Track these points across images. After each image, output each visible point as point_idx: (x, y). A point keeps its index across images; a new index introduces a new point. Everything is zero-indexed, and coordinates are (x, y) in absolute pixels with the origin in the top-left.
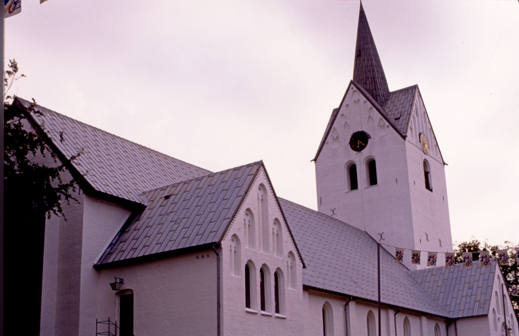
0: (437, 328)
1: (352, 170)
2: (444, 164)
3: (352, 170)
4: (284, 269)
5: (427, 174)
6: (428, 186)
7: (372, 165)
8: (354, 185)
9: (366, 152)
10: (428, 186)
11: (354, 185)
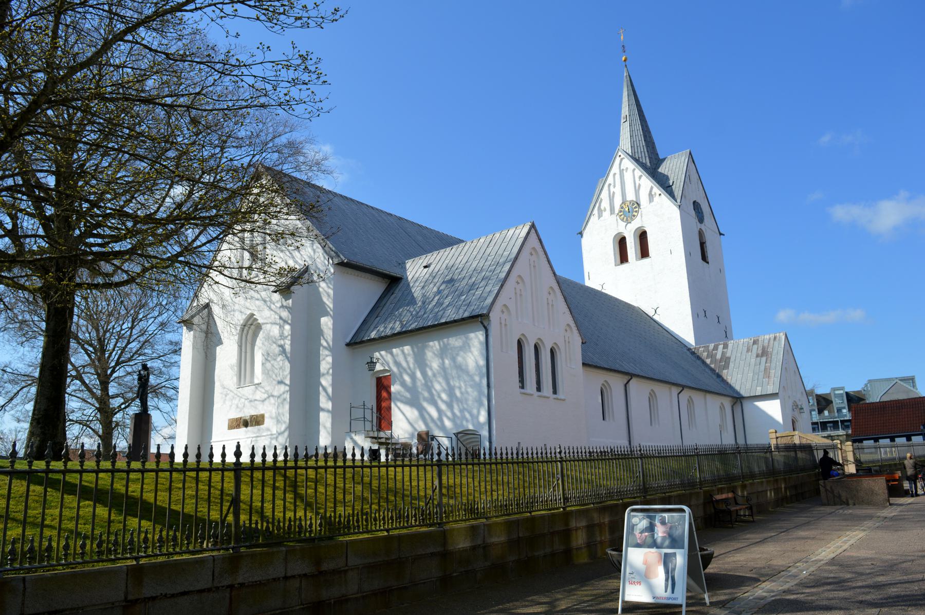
0: (722, 408)
1: (622, 243)
2: (721, 234)
3: (622, 243)
4: (561, 345)
5: (702, 245)
6: (704, 258)
7: (643, 237)
8: (623, 258)
9: (635, 224)
10: (704, 258)
11: (623, 258)
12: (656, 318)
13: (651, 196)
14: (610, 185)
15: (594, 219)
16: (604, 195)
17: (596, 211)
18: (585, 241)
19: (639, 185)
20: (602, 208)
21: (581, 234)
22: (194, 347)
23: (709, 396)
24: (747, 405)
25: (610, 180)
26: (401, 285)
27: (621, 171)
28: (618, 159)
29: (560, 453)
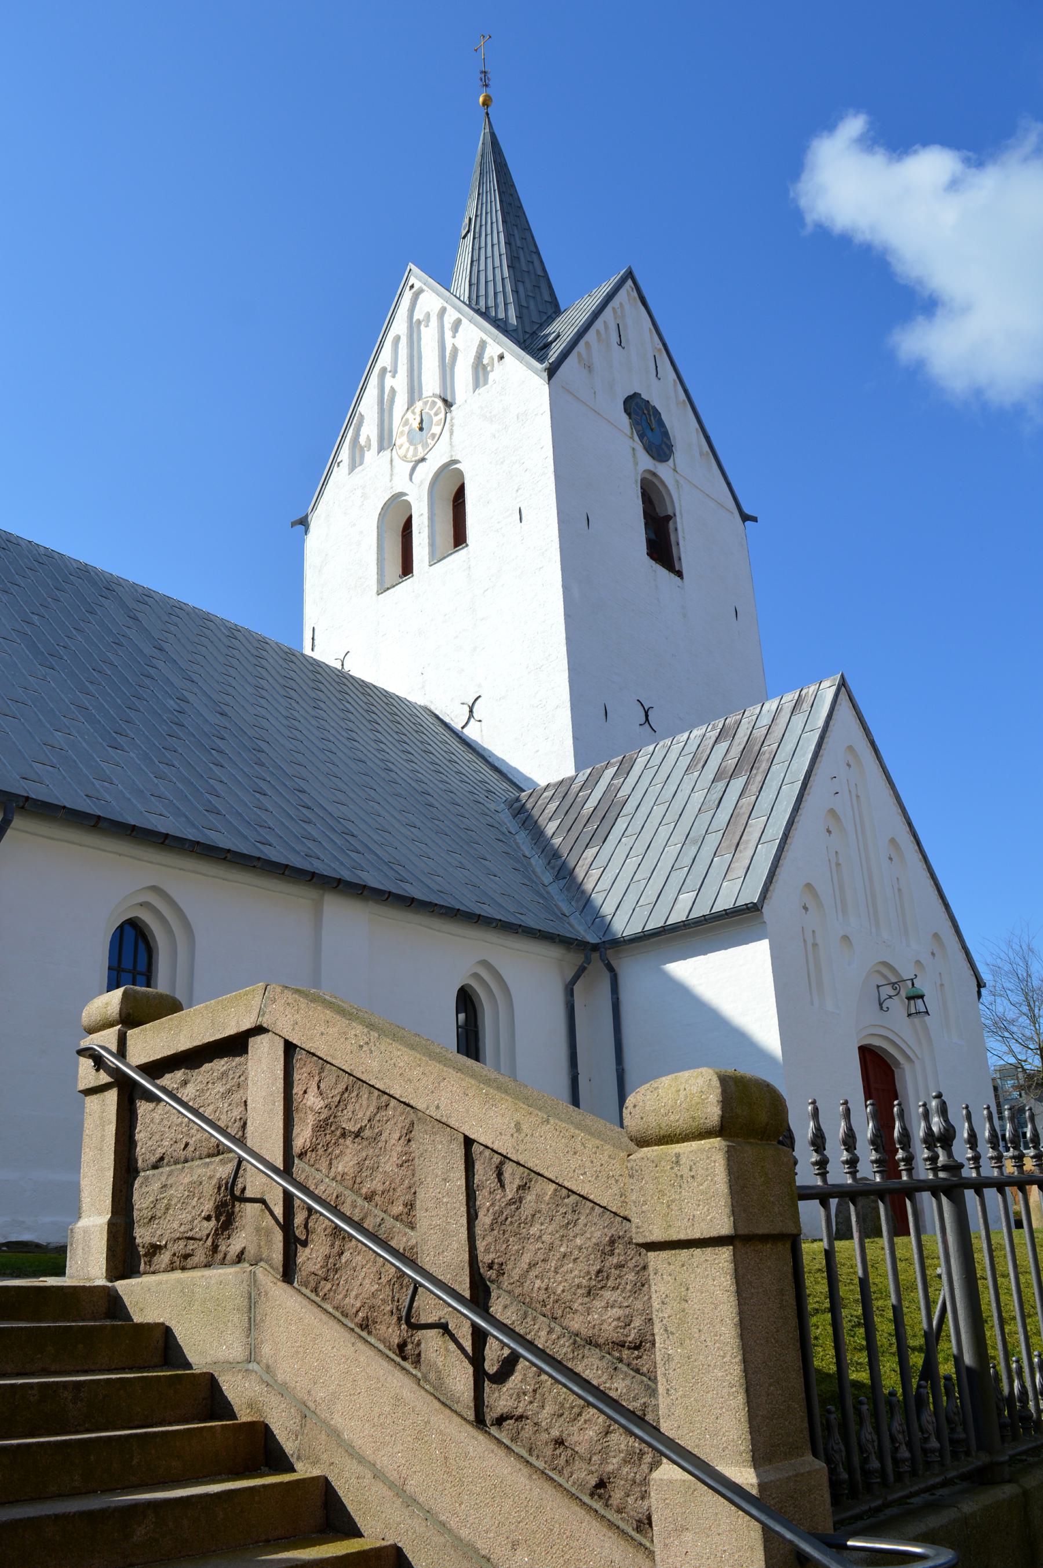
2: (745, 518)
12: (472, 732)
13: (480, 371)
14: (384, 370)
15: (339, 475)
16: (368, 405)
17: (344, 455)
18: (314, 542)
19: (455, 350)
20: (362, 440)
21: (304, 523)
22: (907, 1095)
23: (342, 916)
24: (634, 975)
25: (385, 359)
26: (876, 1042)
27: (414, 327)
28: (408, 295)
29: (947, 1138)
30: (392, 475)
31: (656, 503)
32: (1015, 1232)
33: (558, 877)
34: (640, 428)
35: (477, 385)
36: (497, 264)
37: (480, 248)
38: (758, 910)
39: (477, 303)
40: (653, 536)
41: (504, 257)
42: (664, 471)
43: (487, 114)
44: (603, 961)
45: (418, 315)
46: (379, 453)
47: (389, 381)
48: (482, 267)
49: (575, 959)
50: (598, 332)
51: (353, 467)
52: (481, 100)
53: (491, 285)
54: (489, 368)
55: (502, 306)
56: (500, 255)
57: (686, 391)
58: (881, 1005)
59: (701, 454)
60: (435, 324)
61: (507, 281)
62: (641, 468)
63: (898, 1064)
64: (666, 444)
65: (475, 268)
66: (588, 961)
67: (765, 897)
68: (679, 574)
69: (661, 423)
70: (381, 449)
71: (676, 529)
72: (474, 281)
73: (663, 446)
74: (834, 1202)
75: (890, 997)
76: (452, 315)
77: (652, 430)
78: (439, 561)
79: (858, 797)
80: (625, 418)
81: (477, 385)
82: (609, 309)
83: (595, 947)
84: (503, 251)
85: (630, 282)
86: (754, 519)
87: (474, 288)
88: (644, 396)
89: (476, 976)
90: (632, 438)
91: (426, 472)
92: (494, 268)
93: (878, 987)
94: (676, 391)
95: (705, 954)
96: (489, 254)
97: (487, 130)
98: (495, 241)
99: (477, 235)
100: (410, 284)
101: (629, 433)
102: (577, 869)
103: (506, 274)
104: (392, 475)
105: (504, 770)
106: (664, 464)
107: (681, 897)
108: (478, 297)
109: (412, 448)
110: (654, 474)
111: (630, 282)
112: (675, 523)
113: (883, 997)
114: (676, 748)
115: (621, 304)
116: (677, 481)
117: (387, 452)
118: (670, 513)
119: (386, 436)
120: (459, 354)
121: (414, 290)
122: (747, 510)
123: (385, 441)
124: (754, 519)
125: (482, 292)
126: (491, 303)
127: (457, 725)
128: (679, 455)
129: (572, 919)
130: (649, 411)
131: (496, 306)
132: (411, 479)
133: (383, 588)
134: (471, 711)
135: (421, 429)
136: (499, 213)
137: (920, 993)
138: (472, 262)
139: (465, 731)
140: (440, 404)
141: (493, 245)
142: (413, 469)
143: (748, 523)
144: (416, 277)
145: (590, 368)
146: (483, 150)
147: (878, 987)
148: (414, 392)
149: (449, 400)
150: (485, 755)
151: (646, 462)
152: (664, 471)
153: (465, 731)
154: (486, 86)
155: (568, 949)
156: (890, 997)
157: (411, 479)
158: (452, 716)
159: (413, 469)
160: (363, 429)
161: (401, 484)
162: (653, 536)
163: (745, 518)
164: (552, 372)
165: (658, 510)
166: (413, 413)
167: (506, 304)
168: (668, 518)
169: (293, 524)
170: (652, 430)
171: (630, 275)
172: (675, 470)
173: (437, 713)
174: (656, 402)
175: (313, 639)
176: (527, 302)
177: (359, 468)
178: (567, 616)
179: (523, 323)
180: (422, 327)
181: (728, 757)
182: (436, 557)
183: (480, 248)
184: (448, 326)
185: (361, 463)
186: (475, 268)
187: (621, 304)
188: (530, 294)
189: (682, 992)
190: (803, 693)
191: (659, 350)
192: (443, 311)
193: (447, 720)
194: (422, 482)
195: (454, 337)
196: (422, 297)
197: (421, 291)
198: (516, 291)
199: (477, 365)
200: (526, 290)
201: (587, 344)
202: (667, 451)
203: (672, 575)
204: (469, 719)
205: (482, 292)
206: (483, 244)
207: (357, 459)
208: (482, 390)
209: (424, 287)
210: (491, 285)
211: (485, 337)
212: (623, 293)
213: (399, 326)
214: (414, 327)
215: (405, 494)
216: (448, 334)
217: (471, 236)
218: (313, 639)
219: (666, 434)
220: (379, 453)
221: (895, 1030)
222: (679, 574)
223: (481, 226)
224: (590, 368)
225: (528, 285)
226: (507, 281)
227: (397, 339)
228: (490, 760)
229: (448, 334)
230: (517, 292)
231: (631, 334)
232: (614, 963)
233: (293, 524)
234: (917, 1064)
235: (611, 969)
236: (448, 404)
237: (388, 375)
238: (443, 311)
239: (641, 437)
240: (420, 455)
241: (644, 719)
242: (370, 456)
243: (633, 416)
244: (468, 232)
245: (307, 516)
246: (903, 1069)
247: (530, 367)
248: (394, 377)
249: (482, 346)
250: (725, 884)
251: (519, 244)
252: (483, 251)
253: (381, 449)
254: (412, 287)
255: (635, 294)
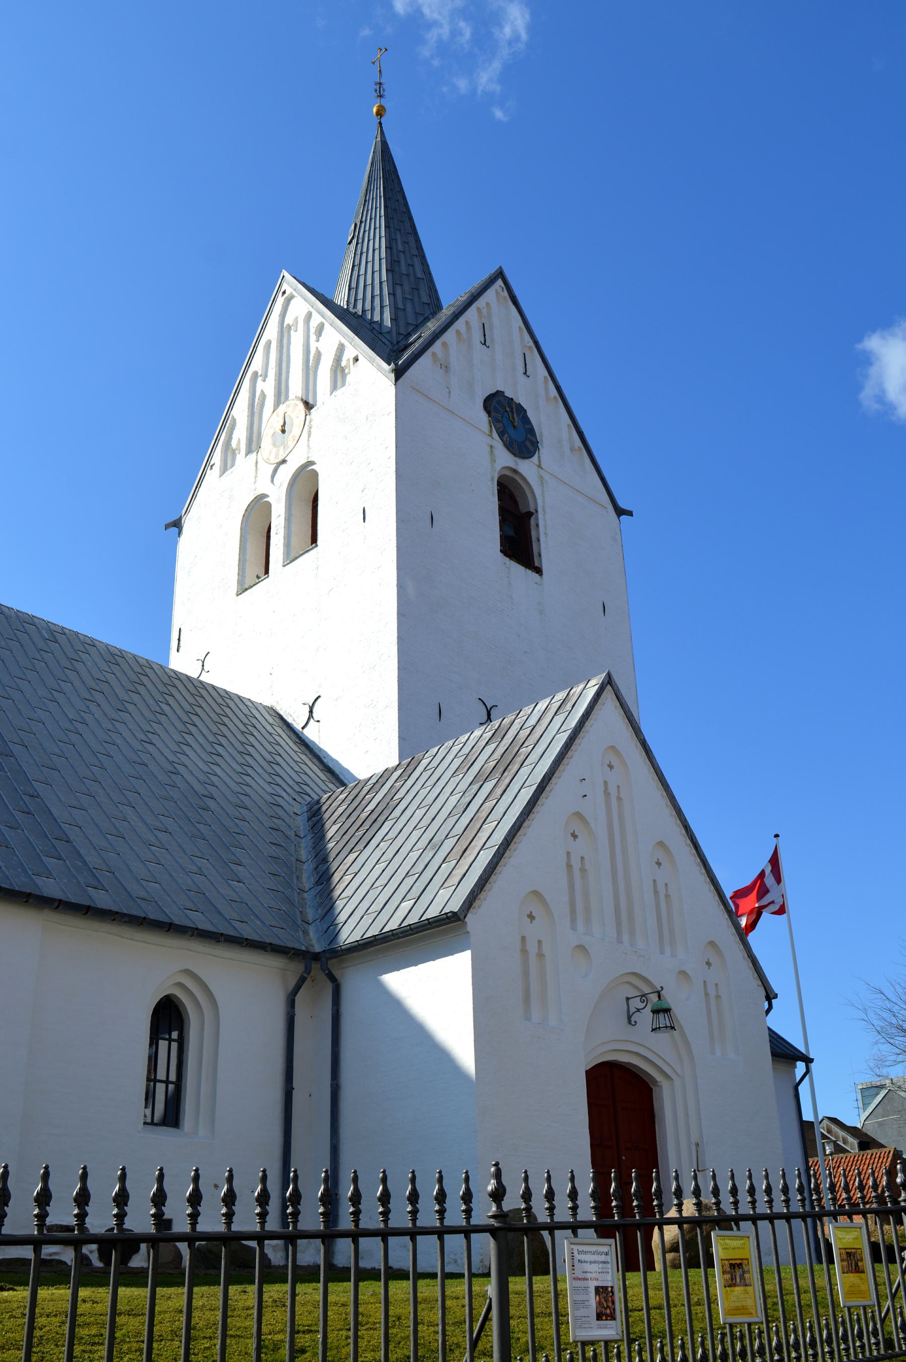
2: (620, 512)
12: (311, 733)
14: (255, 374)
15: (212, 476)
16: (240, 411)
17: (217, 458)
20: (234, 444)
21: (177, 524)
25: (257, 364)
27: (284, 331)
28: (280, 300)
30: (256, 477)
31: (519, 499)
32: (816, 1267)
33: (318, 883)
34: (499, 425)
35: (334, 388)
36: (377, 268)
37: (361, 253)
38: (459, 919)
39: (355, 307)
40: (511, 533)
41: (384, 261)
42: (527, 468)
43: (380, 123)
44: (324, 971)
45: (289, 320)
46: (246, 455)
47: (260, 385)
48: (362, 272)
49: (296, 969)
50: (458, 332)
51: (224, 469)
52: (375, 110)
53: (369, 289)
54: (347, 371)
55: (378, 309)
56: (380, 259)
57: (558, 388)
58: (629, 1018)
59: (572, 449)
60: (301, 326)
61: (385, 285)
62: (499, 466)
63: (655, 1082)
64: (531, 441)
65: (356, 273)
66: (308, 970)
67: (470, 906)
68: (539, 571)
69: (526, 420)
70: (249, 451)
71: (537, 526)
72: (354, 285)
73: (527, 443)
74: (809, 1220)
75: (638, 1010)
76: (316, 320)
77: (514, 427)
78: (291, 562)
79: (619, 799)
80: (484, 417)
81: (334, 388)
82: (472, 310)
83: (316, 957)
84: (383, 255)
85: (500, 282)
86: (630, 513)
87: (353, 292)
88: (508, 394)
89: (180, 985)
90: (491, 435)
91: (286, 473)
92: (373, 272)
93: (628, 999)
94: (547, 389)
95: (416, 965)
96: (370, 259)
97: (379, 139)
98: (377, 246)
99: (360, 241)
100: (282, 290)
101: (487, 430)
102: (335, 875)
103: (384, 278)
104: (256, 477)
105: (337, 771)
106: (527, 461)
107: (402, 904)
108: (356, 300)
109: (275, 449)
110: (515, 471)
111: (500, 282)
112: (537, 519)
113: (632, 1010)
114: (456, 749)
115: (487, 304)
116: (541, 477)
117: (254, 455)
118: (532, 509)
119: (255, 439)
120: (322, 358)
121: (285, 296)
122: (622, 504)
123: (253, 444)
124: (630, 513)
125: (360, 296)
126: (368, 306)
127: (298, 726)
128: (546, 451)
129: (311, 930)
130: (512, 409)
131: (373, 309)
132: (272, 481)
133: (243, 589)
134: (311, 712)
135: (283, 431)
136: (383, 218)
137: (665, 1006)
138: (353, 266)
139: (306, 731)
140: (301, 406)
141: (374, 250)
142: (275, 471)
143: (623, 517)
144: (288, 284)
145: (446, 368)
146: (373, 158)
147: (628, 999)
148: (281, 395)
149: (311, 402)
150: (321, 756)
151: (505, 459)
152: (527, 468)
153: (306, 731)
154: (381, 96)
155: (291, 958)
156: (638, 1010)
157: (272, 481)
158: (294, 716)
159: (275, 471)
160: (235, 432)
161: (264, 487)
162: (511, 533)
163: (620, 512)
164: (399, 373)
165: (521, 507)
166: (278, 415)
167: (382, 307)
168: (530, 514)
169: (167, 527)
170: (514, 427)
171: (500, 274)
172: (539, 466)
173: (282, 713)
174: (522, 399)
175: (179, 640)
176: (404, 304)
177: (229, 471)
178: (401, 615)
179: (398, 326)
180: (292, 332)
181: (491, 759)
182: (290, 558)
183: (361, 253)
184: (312, 330)
185: (233, 465)
186: (356, 273)
187: (487, 304)
188: (408, 297)
189: (395, 1006)
190: (572, 692)
191: (530, 348)
192: (309, 316)
193: (290, 720)
194: (281, 484)
195: (318, 341)
196: (292, 302)
197: (291, 297)
198: (392, 294)
199: (336, 368)
200: (403, 292)
201: (445, 344)
202: (531, 448)
203: (529, 572)
204: (309, 719)
205: (360, 296)
206: (365, 250)
207: (229, 462)
208: (339, 392)
209: (295, 294)
210: (369, 289)
211: (343, 341)
212: (490, 294)
213: (271, 332)
214: (284, 331)
215: (267, 496)
216: (313, 337)
217: (354, 242)
218: (179, 640)
219: (531, 431)
220: (246, 455)
221: (642, 1047)
222: (539, 571)
223: (364, 232)
224: (446, 368)
225: (407, 288)
226: (385, 285)
227: (269, 343)
228: (325, 760)
229: (313, 337)
230: (394, 295)
231: (497, 334)
232: (336, 973)
233: (167, 527)
234: (677, 1082)
235: (333, 979)
236: (308, 406)
237: (260, 379)
238: (309, 316)
239: (501, 435)
240: (281, 458)
241: (485, 718)
242: (240, 457)
243: (493, 414)
244: (353, 238)
245: (180, 518)
246: (661, 1087)
247: (380, 369)
248: (264, 381)
249: (341, 348)
250: (441, 891)
251: (400, 248)
252: (364, 255)
253: (249, 451)
254: (284, 293)
255: (506, 293)
